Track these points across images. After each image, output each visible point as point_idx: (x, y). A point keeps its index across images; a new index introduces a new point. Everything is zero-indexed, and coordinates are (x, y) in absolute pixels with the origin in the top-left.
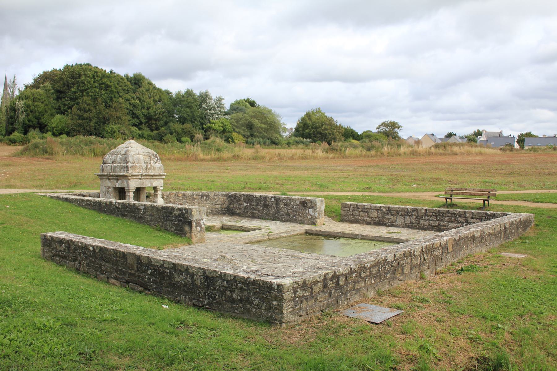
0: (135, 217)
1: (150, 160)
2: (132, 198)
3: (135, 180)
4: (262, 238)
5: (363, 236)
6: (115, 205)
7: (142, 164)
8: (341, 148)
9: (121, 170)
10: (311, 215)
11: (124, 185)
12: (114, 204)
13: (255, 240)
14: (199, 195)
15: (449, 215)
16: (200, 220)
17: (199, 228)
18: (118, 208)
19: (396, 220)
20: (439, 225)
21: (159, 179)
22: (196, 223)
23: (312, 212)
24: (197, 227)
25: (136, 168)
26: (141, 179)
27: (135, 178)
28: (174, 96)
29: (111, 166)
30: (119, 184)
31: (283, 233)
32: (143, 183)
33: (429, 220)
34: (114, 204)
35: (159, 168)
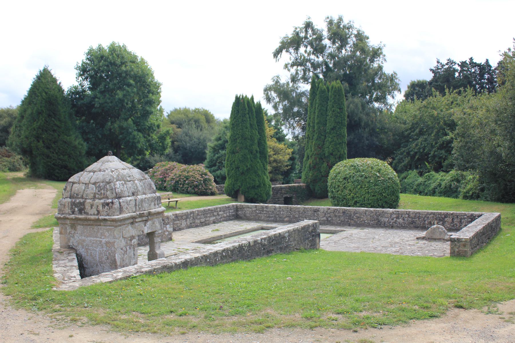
0: (281, 248)
5: (225, 235)
6: (261, 243)
9: (150, 205)
10: (168, 231)
11: (156, 226)
12: (260, 241)
15: (210, 212)
18: (265, 245)
19: (181, 224)
20: (205, 221)
23: (169, 228)
28: (65, 93)
29: (136, 200)
30: (148, 228)
33: (200, 218)
34: (260, 241)
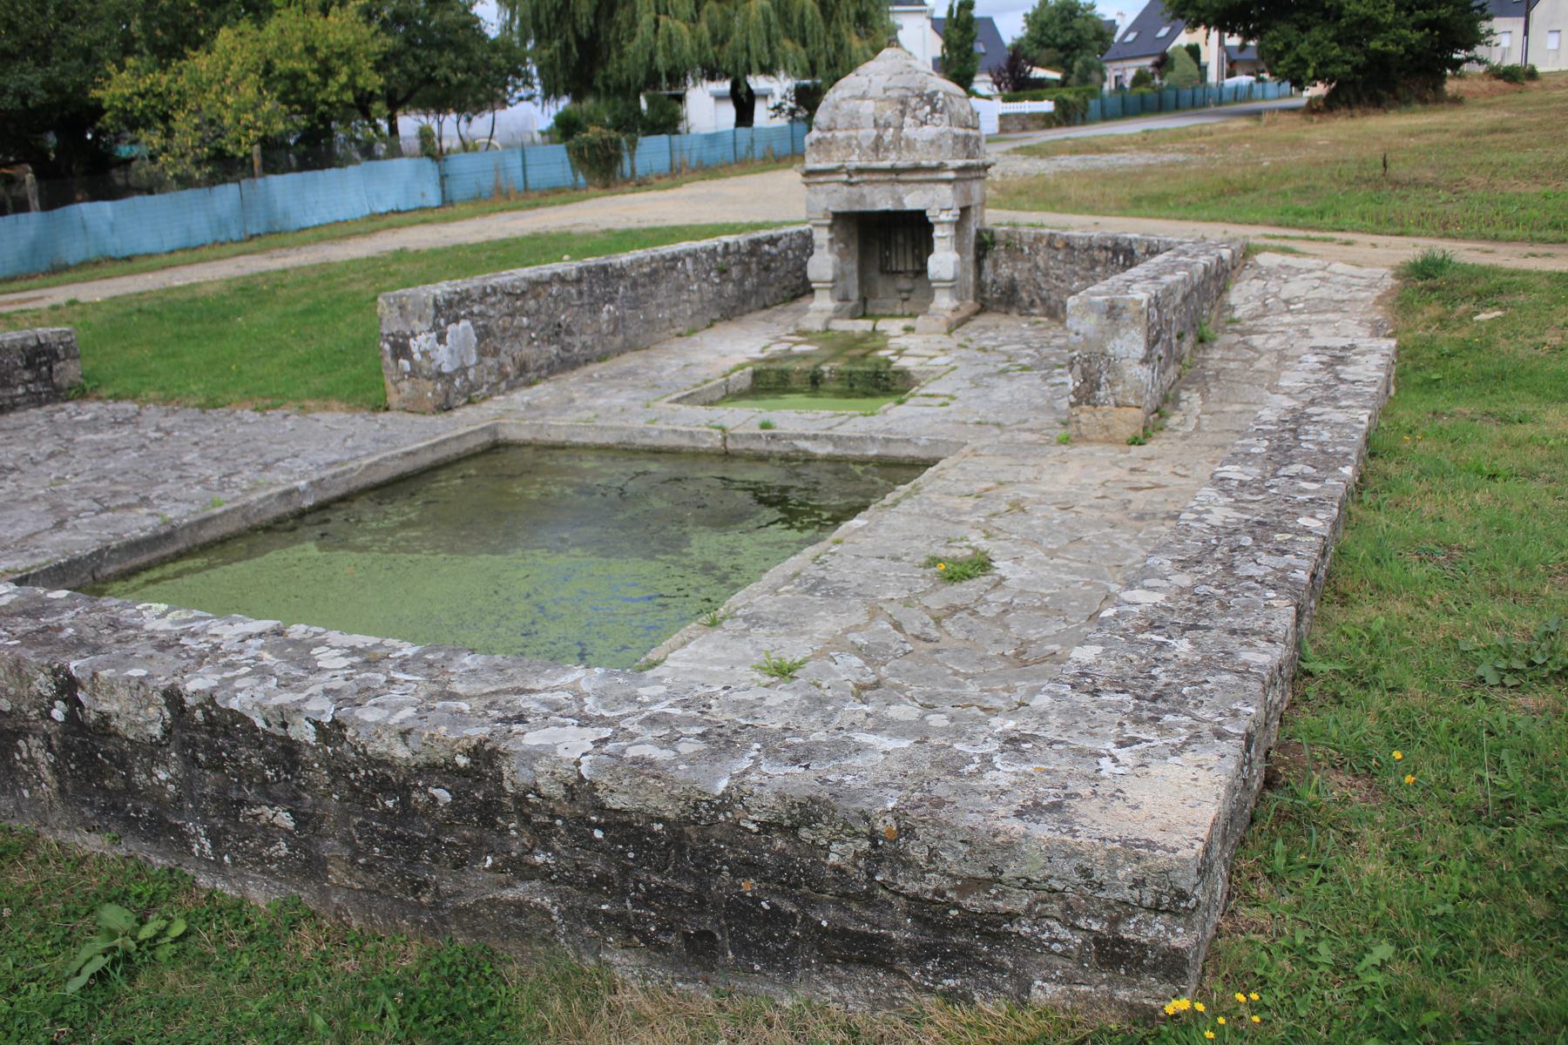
1: (903, 113)
2: (821, 247)
3: (825, 187)
4: (685, 442)
7: (861, 132)
8: (335, 62)
13: (648, 441)
14: (1106, 249)
16: (407, 338)
17: (405, 364)
21: (929, 181)
22: (394, 345)
24: (396, 357)
25: (833, 147)
26: (851, 184)
27: (822, 179)
31: (815, 437)
32: (862, 196)
35: (932, 143)
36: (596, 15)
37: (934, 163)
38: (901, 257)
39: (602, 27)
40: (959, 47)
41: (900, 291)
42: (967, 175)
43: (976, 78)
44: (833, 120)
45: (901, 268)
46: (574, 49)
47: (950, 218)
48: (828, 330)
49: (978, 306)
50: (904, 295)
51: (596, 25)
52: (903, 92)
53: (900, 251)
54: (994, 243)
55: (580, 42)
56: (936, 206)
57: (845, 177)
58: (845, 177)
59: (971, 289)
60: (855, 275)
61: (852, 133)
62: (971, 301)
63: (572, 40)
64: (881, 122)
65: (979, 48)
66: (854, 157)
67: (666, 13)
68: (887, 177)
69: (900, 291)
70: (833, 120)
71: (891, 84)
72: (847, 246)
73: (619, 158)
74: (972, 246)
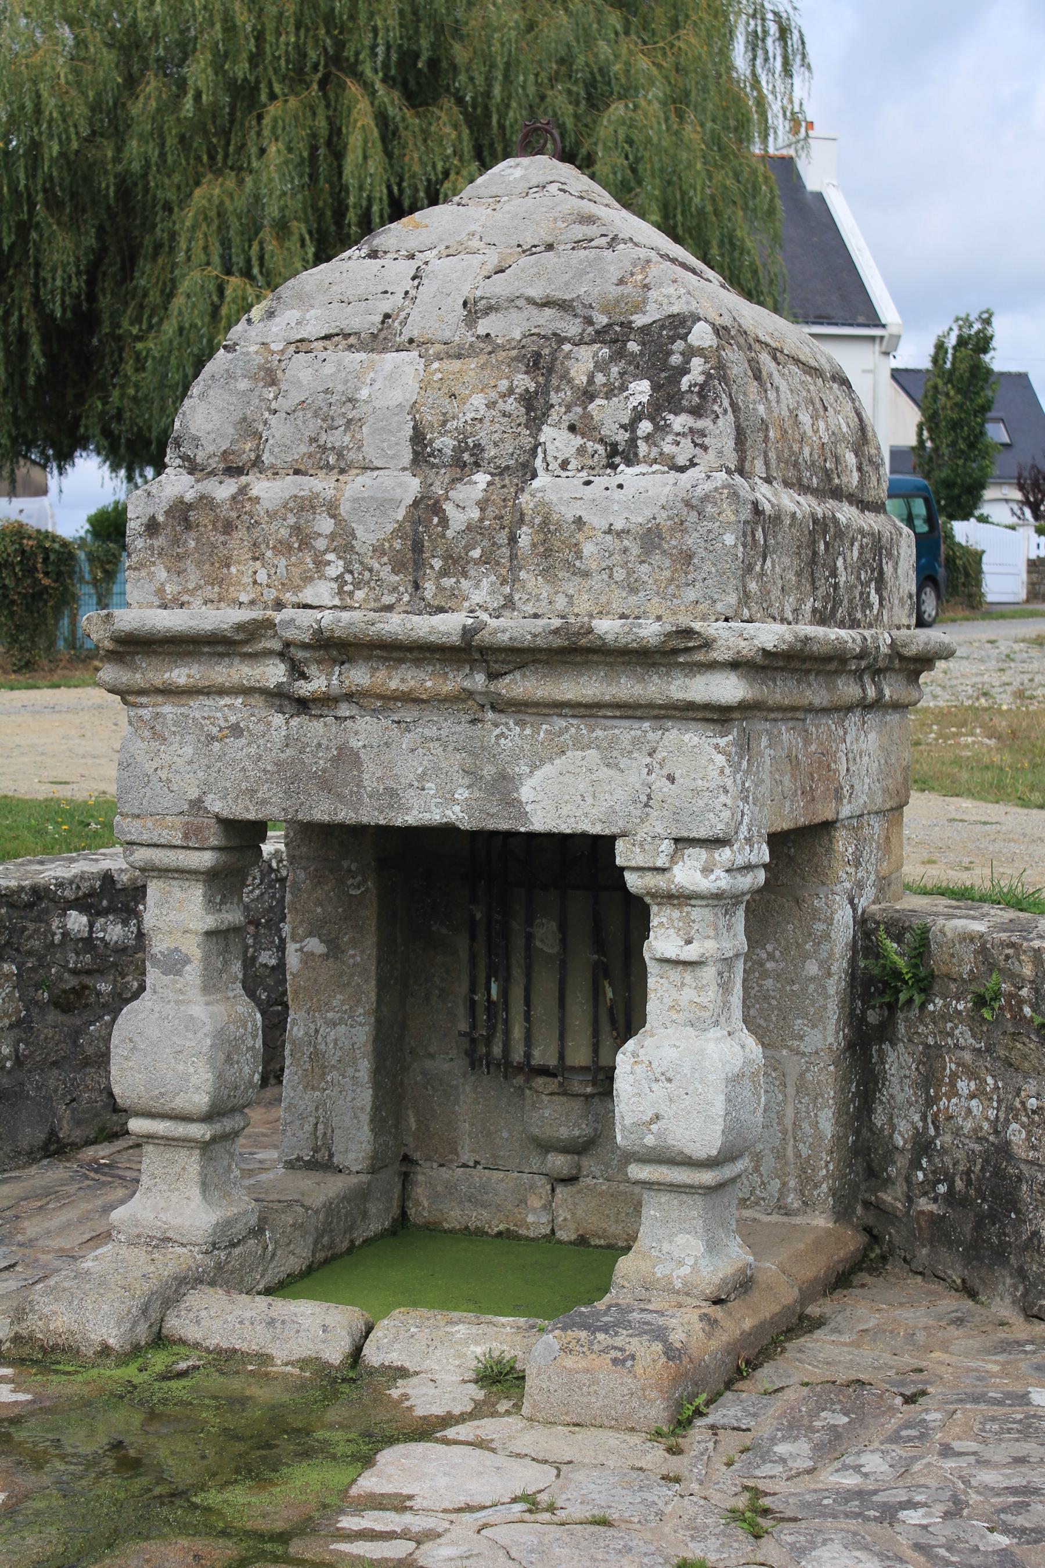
2: (174, 964)
3: (198, 708)
7: (357, 485)
25: (239, 542)
26: (303, 705)
27: (180, 675)
36: (93, 273)
37: (650, 631)
38: (544, 1005)
39: (105, 301)
40: (955, 425)
41: (546, 1147)
42: (816, 694)
43: (988, 494)
44: (248, 429)
45: (544, 1054)
46: (35, 348)
47: (720, 881)
48: (160, 1340)
49: (852, 1241)
50: (559, 1162)
51: (92, 298)
52: (548, 320)
53: (546, 984)
54: (926, 984)
55: (50, 329)
56: (658, 824)
57: (275, 673)
58: (275, 673)
59: (825, 1167)
60: (364, 1068)
61: (321, 485)
62: (821, 1221)
63: (31, 326)
64: (446, 443)
65: (997, 433)
66: (322, 592)
67: (247, 274)
68: (454, 681)
69: (546, 1147)
70: (248, 429)
71: (500, 287)
72: (334, 949)
73: (66, 600)
74: (835, 985)
